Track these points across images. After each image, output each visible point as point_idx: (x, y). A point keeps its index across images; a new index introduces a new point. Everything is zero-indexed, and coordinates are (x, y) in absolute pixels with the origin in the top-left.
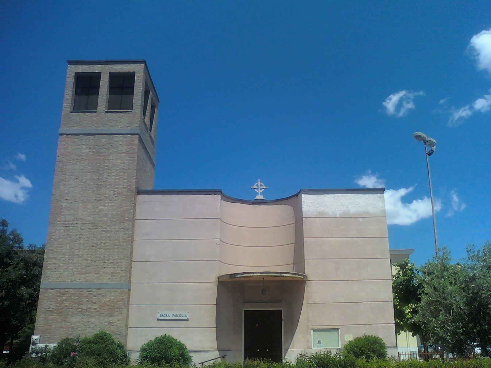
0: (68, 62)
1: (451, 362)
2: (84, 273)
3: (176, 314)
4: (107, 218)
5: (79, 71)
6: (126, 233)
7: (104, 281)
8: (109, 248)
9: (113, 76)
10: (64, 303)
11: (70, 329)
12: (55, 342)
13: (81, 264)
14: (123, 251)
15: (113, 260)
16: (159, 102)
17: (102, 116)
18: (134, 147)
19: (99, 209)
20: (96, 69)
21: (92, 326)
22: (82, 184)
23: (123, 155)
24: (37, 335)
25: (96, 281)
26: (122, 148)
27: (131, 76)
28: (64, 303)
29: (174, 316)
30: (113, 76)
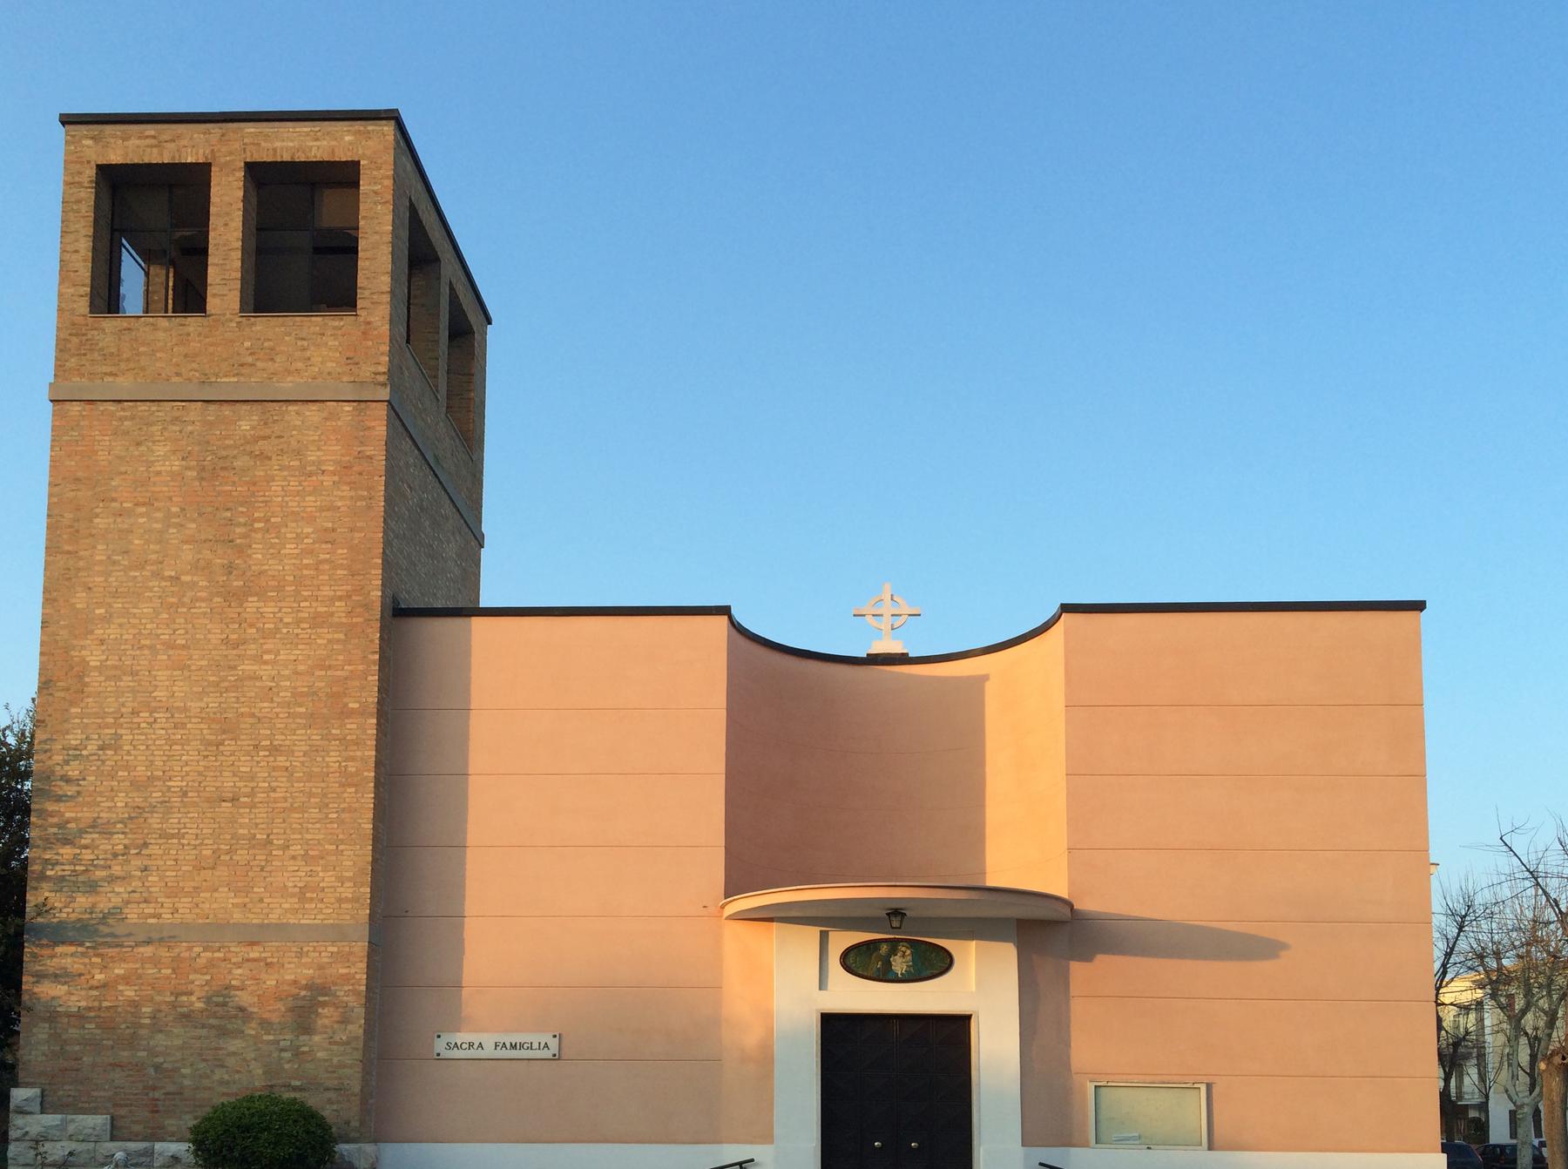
0: (63, 123)
1: (16, 784)
2: (191, 890)
3: (509, 1039)
4: (275, 705)
5: (115, 157)
6: (351, 753)
7: (273, 918)
8: (286, 805)
9: (260, 175)
10: (120, 988)
11: (152, 1071)
12: (100, 1111)
13: (176, 860)
14: (343, 816)
15: (305, 847)
16: (490, 323)
17: (228, 335)
18: (369, 451)
19: (240, 673)
20: (187, 147)
21: (231, 1062)
22: (164, 584)
23: (328, 481)
24: (28, 1085)
25: (237, 916)
26: (319, 453)
27: (344, 176)
28: (120, 988)
29: (498, 1048)
30: (260, 175)
